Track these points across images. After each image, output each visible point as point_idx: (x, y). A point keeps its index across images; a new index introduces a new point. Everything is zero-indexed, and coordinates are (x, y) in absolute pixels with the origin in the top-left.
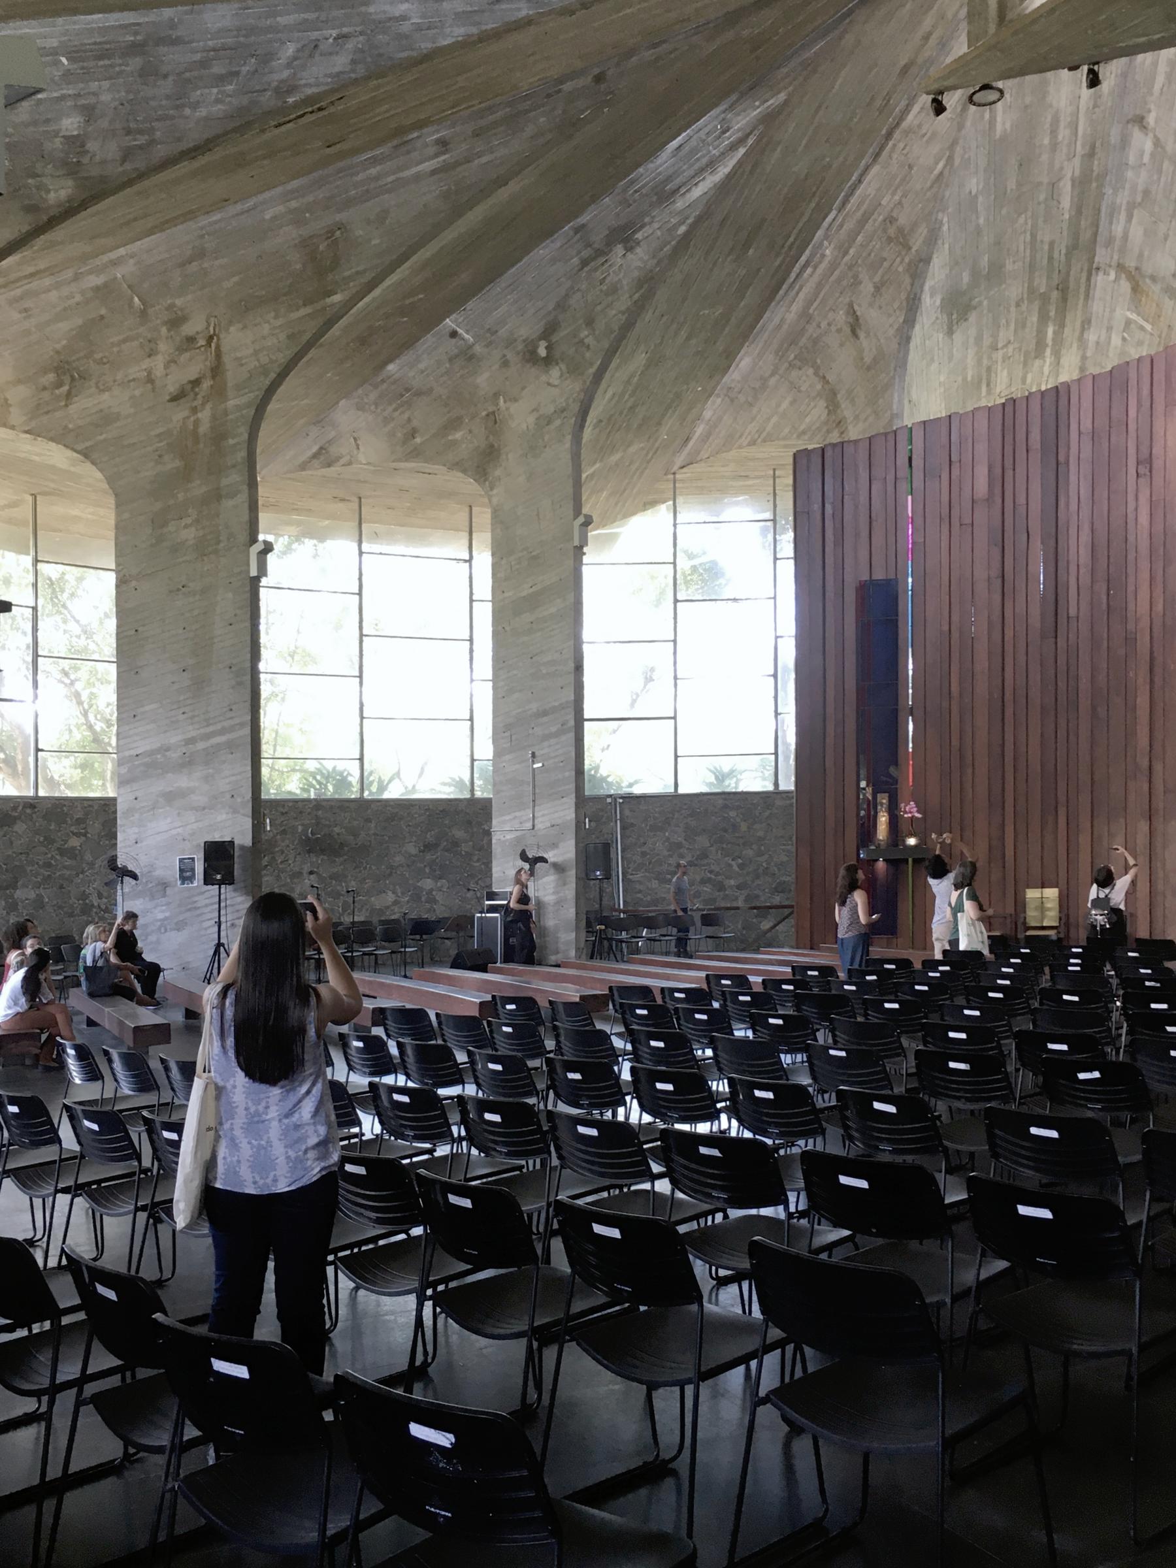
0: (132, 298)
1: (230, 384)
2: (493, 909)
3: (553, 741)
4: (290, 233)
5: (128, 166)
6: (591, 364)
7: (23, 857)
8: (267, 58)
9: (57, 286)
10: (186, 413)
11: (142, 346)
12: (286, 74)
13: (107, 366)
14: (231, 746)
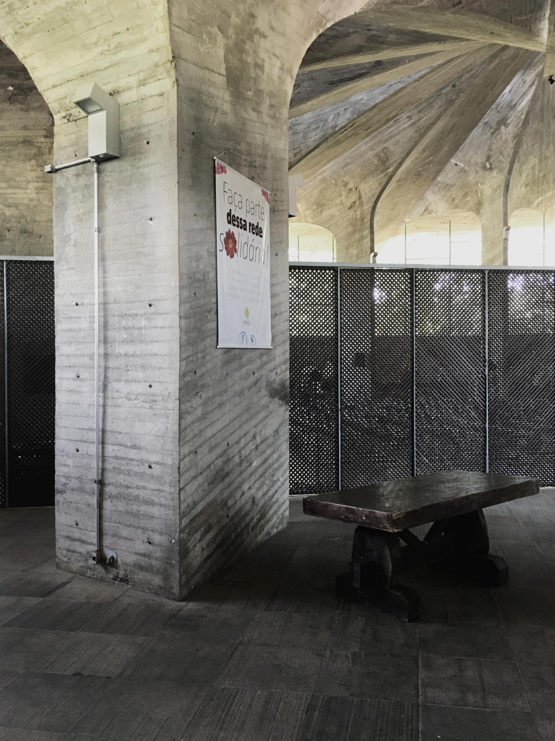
4: (372, 153)
5: (296, 158)
6: (506, 168)
8: (326, 120)
9: (310, 181)
10: (353, 212)
11: (338, 194)
12: (333, 123)
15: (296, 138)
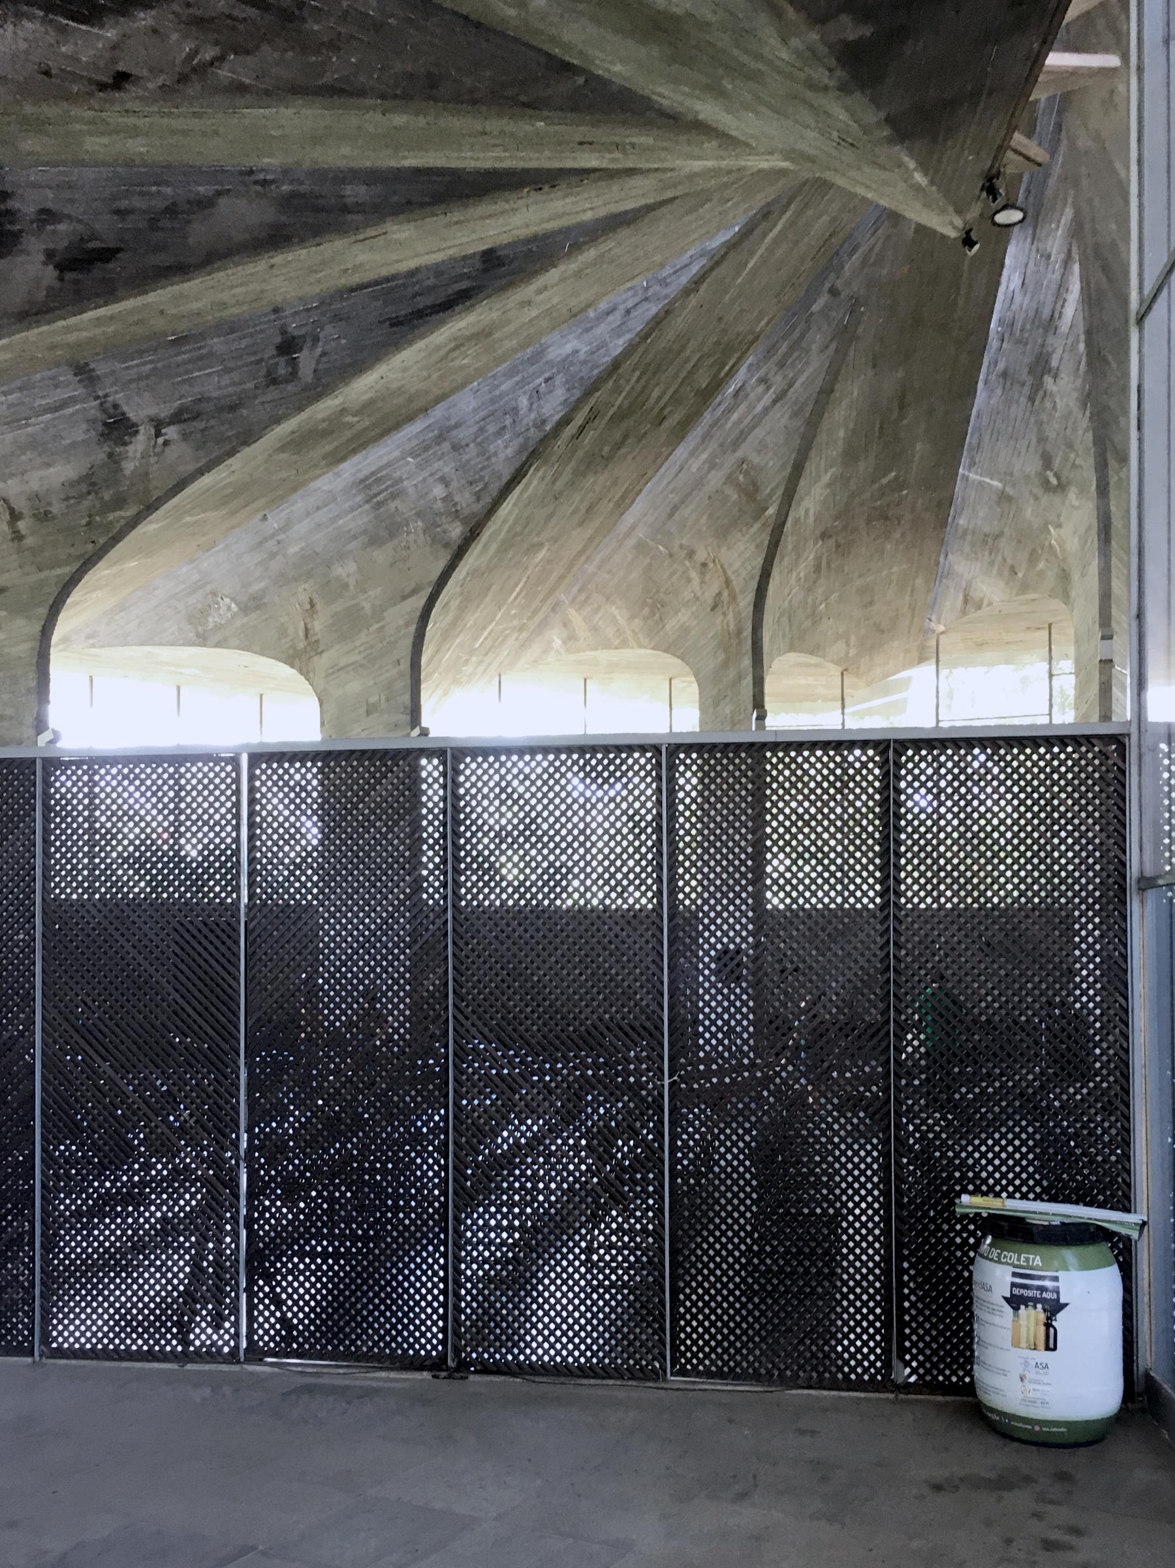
4: (715, 479)
8: (515, 410)
15: (466, 457)
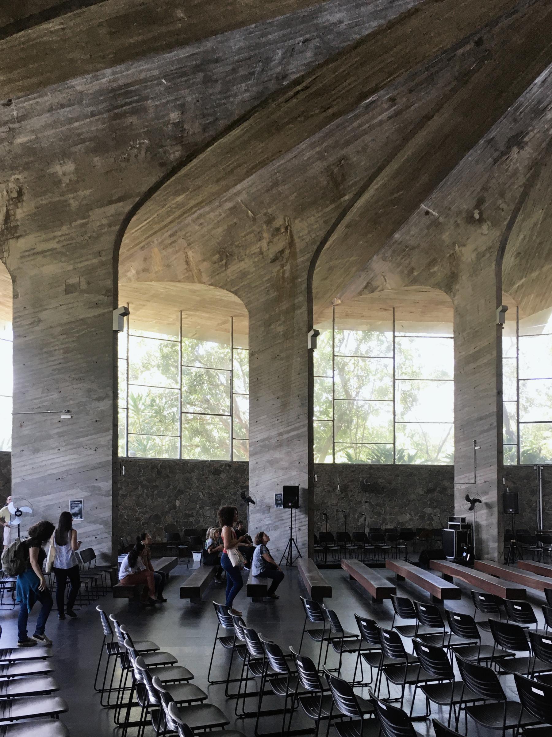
0: (248, 212)
1: (298, 250)
2: (452, 527)
3: (485, 434)
4: (319, 166)
5: (207, 135)
6: (505, 219)
7: (224, 490)
8: (269, 60)
9: (213, 210)
10: (279, 268)
11: (255, 236)
13: (241, 248)
14: (299, 437)
